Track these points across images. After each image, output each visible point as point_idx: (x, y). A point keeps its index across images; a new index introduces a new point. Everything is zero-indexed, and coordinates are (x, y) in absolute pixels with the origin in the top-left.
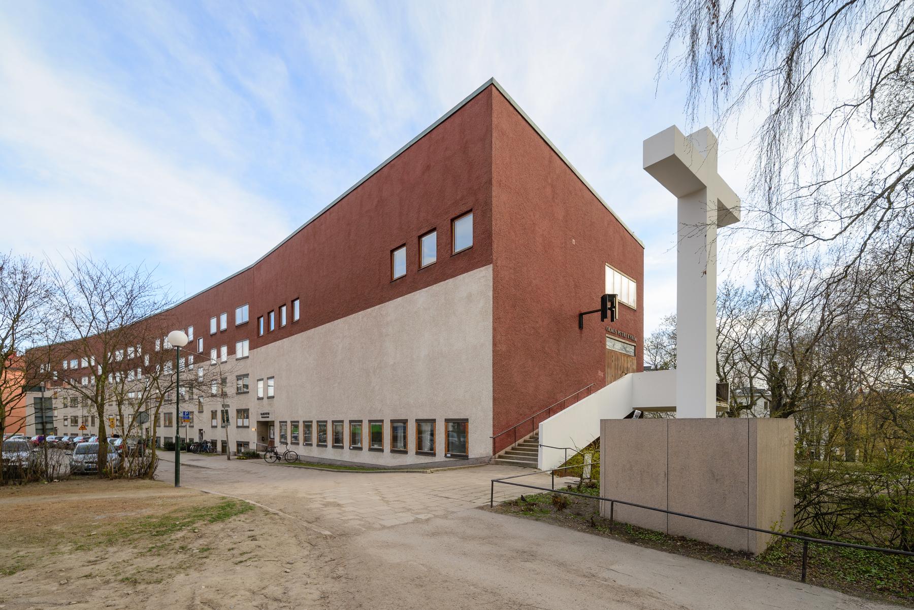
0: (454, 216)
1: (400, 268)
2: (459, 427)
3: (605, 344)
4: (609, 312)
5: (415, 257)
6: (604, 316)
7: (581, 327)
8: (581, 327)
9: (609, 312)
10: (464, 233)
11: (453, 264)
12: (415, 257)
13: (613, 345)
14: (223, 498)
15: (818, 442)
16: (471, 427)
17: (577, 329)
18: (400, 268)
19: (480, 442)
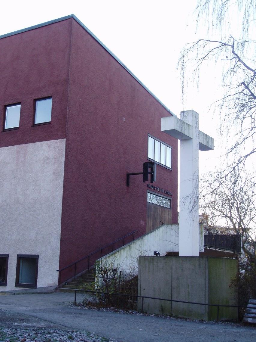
0: (37, 98)
1: (13, 118)
2: (30, 263)
3: (146, 199)
4: (149, 175)
5: (28, 114)
6: (145, 179)
7: (128, 184)
8: (128, 184)
9: (149, 175)
10: (44, 113)
11: (31, 132)
12: (28, 114)
13: (152, 199)
14: (199, 234)
15: (19, 326)
16: (40, 262)
17: (125, 186)
18: (13, 118)
19: (48, 275)
